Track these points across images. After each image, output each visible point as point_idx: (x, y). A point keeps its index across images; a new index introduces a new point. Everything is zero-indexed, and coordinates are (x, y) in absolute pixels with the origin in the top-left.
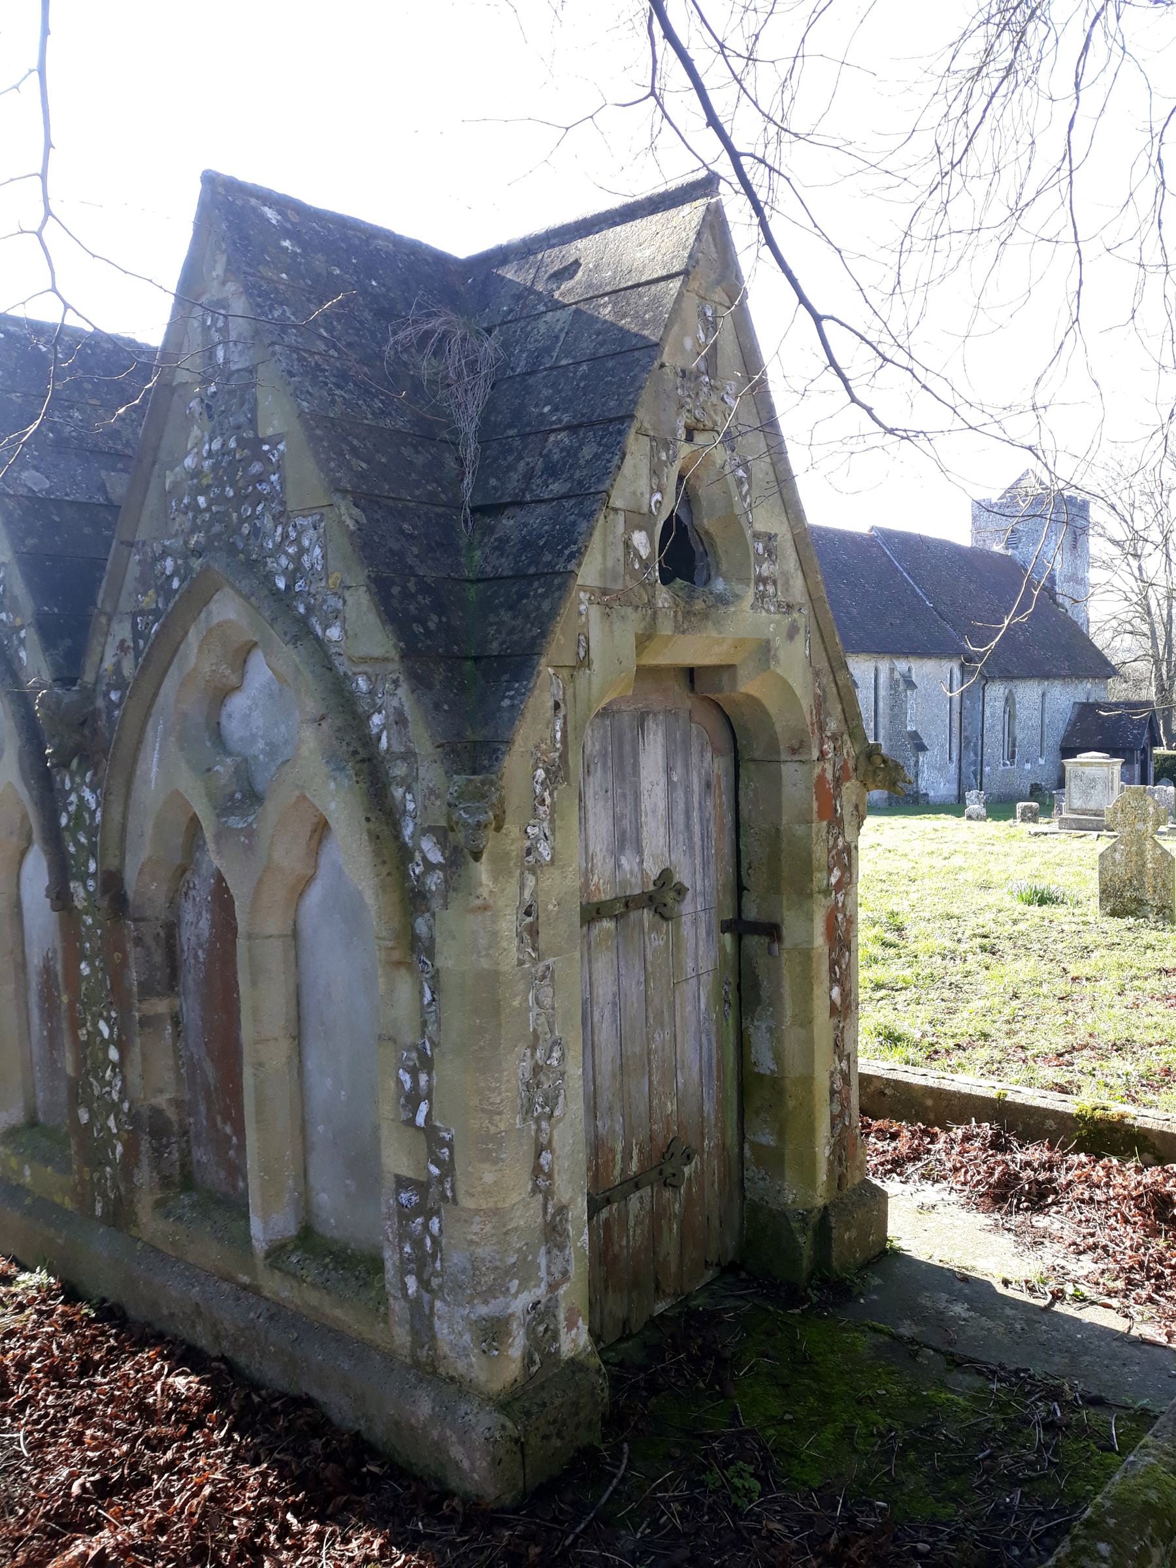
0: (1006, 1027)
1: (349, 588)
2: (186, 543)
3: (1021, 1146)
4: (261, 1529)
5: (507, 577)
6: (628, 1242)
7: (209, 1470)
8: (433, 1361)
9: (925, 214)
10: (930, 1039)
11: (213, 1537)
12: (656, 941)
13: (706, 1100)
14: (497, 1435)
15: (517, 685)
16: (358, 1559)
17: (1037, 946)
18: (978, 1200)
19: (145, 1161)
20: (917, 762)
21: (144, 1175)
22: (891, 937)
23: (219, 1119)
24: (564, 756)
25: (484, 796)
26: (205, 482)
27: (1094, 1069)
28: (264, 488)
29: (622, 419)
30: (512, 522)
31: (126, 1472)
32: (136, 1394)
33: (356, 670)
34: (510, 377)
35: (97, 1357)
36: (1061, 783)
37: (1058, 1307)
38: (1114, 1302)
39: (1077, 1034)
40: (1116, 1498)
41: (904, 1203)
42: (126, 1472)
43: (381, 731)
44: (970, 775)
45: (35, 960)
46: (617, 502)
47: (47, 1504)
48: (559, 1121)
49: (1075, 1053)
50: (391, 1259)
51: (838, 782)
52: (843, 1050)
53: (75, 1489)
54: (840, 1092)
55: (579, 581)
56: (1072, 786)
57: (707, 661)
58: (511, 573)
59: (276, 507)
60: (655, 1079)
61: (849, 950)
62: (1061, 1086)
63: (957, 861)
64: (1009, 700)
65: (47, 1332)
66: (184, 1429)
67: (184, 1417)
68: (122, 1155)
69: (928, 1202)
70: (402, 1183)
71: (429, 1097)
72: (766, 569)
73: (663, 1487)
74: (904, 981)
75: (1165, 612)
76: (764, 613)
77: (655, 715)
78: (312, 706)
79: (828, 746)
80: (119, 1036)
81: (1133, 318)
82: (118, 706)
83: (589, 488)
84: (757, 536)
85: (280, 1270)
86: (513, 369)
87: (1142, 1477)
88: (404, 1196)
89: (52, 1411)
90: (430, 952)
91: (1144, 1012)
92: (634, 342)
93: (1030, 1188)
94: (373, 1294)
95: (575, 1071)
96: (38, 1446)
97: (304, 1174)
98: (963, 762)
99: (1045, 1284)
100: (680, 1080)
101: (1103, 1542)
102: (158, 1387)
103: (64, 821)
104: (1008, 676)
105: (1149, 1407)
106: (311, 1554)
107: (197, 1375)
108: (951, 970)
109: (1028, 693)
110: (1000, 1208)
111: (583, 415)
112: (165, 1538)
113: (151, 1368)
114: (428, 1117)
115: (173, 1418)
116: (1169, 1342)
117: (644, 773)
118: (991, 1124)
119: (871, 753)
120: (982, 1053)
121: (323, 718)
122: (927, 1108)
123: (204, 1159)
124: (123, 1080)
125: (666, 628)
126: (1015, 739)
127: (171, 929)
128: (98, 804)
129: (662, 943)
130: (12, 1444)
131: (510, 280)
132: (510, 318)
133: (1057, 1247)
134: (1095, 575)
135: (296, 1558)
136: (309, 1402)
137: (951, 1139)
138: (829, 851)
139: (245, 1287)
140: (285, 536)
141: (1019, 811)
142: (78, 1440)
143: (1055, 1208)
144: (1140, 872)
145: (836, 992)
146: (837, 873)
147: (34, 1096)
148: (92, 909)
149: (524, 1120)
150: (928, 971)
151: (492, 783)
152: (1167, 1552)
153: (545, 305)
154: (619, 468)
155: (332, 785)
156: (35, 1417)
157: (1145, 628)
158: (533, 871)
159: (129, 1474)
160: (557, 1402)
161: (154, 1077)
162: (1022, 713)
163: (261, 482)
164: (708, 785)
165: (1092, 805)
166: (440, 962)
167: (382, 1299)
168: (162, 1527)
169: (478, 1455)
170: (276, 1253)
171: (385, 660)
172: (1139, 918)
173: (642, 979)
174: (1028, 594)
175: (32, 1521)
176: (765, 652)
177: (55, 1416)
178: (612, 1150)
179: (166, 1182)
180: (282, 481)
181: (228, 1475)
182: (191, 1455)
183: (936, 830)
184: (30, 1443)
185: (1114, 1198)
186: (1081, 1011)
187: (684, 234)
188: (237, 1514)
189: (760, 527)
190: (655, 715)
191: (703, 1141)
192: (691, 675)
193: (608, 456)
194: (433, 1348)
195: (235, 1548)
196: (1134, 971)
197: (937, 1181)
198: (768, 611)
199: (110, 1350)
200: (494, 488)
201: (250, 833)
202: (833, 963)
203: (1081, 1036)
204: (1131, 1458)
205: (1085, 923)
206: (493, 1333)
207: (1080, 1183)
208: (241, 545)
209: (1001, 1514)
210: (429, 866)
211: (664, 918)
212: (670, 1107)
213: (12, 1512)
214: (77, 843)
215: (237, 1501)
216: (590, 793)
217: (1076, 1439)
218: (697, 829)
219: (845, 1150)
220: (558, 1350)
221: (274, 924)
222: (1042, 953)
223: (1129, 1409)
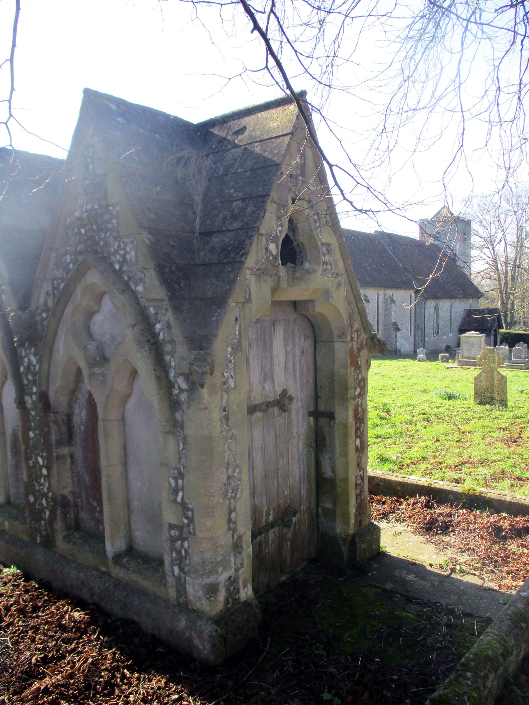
0: (433, 454)
1: (146, 269)
2: (76, 248)
3: (438, 506)
4: (114, 676)
5: (215, 264)
6: (269, 551)
7: (91, 652)
8: (186, 603)
9: (396, 98)
10: (400, 460)
11: (93, 680)
12: (280, 421)
13: (302, 489)
14: (214, 634)
15: (219, 311)
16: (156, 688)
17: (447, 418)
18: (420, 530)
19: (59, 518)
20: (396, 336)
21: (59, 525)
22: (384, 415)
23: (91, 499)
24: (239, 341)
25: (205, 360)
26: (84, 223)
27: (471, 472)
28: (110, 226)
29: (264, 196)
30: (217, 240)
31: (55, 653)
32: (57, 620)
33: (150, 304)
34: (216, 177)
35: (40, 604)
36: (459, 345)
37: (453, 575)
38: (477, 573)
39: (464, 457)
40: (476, 655)
41: (387, 532)
42: (55, 653)
43: (160, 331)
44: (419, 341)
45: (9, 431)
46: (262, 231)
47: (21, 667)
48: (239, 499)
49: (463, 465)
50: (167, 560)
51: (359, 350)
52: (361, 466)
53: (34, 661)
54: (360, 485)
55: (246, 265)
56: (463, 346)
57: (302, 299)
58: (216, 262)
59: (115, 234)
60: (280, 481)
61: (364, 423)
62: (456, 480)
63: (414, 380)
64: (436, 308)
65: (17, 594)
66: (79, 635)
67: (78, 629)
68: (49, 516)
69: (398, 531)
70: (171, 527)
71: (183, 489)
72: (327, 259)
73: (285, 655)
74: (389, 434)
75: (504, 269)
76: (326, 278)
77: (279, 321)
78: (131, 320)
79: (354, 335)
80: (47, 464)
81: (486, 145)
82: (46, 319)
83: (251, 225)
84: (323, 244)
85: (119, 565)
86: (217, 173)
87: (485, 645)
88: (173, 532)
89: (21, 628)
90: (182, 427)
91: (493, 447)
92: (270, 163)
93: (442, 525)
94: (159, 575)
95: (245, 478)
96: (16, 643)
97: (129, 524)
98: (416, 335)
99: (448, 566)
100: (291, 481)
101: (469, 672)
102: (67, 617)
103: (22, 369)
104: (436, 297)
105: (491, 617)
106: (135, 686)
107: (84, 611)
108: (410, 429)
109: (445, 305)
110: (429, 533)
111: (248, 194)
112: (73, 681)
113: (63, 609)
114: (183, 498)
115: (74, 630)
116: (500, 589)
117: (275, 347)
118: (425, 497)
119: (373, 338)
120: (422, 466)
121: (135, 325)
122: (398, 490)
123: (85, 517)
124: (49, 483)
125: (284, 284)
126: (438, 325)
127: (69, 417)
128: (37, 362)
129: (283, 422)
130: (4, 642)
131: (216, 134)
132: (216, 151)
133: (453, 549)
134: (474, 253)
135: (129, 688)
136: (133, 622)
137: (408, 504)
138: (355, 381)
139: (104, 573)
140: (119, 246)
141: (440, 358)
142: (33, 640)
143: (452, 533)
144: (492, 385)
145: (358, 441)
146: (358, 390)
147: (9, 490)
148: (35, 408)
149: (224, 499)
150: (400, 430)
151: (209, 354)
152: (496, 676)
153: (231, 145)
154: (263, 217)
155: (139, 355)
156: (14, 630)
157: (496, 276)
158: (226, 392)
159: (56, 654)
160: (240, 619)
161: (62, 482)
162: (442, 314)
163: (108, 223)
164: (303, 352)
165: (472, 355)
166: (187, 432)
167: (164, 576)
168: (71, 676)
169: (206, 643)
170: (117, 558)
171: (162, 300)
172: (492, 405)
173: (274, 438)
174: (440, 265)
175: (15, 675)
176: (327, 294)
177: (22, 630)
178: (262, 511)
179: (68, 527)
180: (118, 223)
181: (99, 654)
182: (82, 646)
183: (404, 366)
184: (12, 642)
185: (477, 528)
186: (465, 447)
187: (291, 117)
188: (103, 670)
189: (324, 241)
190: (279, 321)
191: (301, 507)
192: (295, 304)
193: (258, 212)
194: (186, 597)
195: (103, 684)
196: (489, 429)
197: (402, 522)
198: (328, 277)
199: (45, 601)
200: (210, 225)
201: (104, 375)
202: (357, 429)
203: (466, 457)
204: (481, 637)
205: (468, 408)
206: (212, 590)
207: (463, 522)
208: (99, 250)
209: (428, 663)
210: (181, 390)
211: (284, 411)
212: (287, 492)
213: (7, 671)
214: (28, 379)
215: (103, 664)
216: (251, 357)
217: (460, 631)
218: (298, 372)
219: (362, 509)
220: (239, 597)
221: (114, 415)
222: (449, 421)
223: (482, 617)
